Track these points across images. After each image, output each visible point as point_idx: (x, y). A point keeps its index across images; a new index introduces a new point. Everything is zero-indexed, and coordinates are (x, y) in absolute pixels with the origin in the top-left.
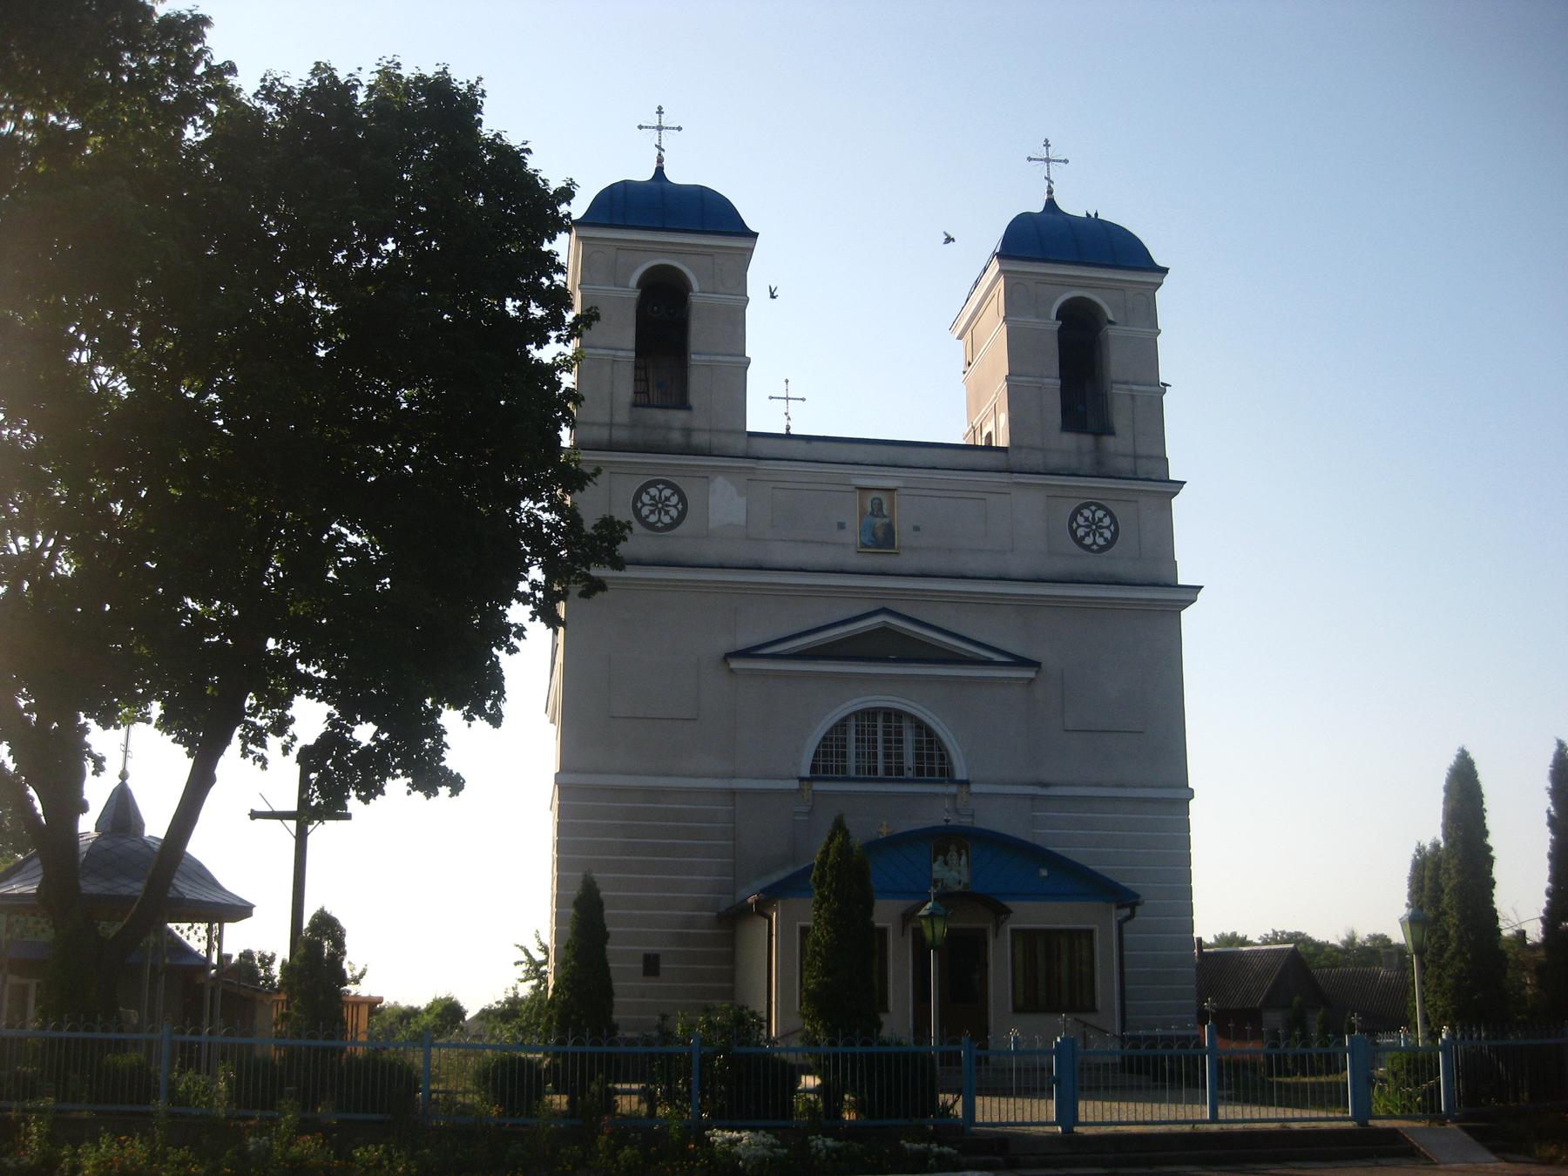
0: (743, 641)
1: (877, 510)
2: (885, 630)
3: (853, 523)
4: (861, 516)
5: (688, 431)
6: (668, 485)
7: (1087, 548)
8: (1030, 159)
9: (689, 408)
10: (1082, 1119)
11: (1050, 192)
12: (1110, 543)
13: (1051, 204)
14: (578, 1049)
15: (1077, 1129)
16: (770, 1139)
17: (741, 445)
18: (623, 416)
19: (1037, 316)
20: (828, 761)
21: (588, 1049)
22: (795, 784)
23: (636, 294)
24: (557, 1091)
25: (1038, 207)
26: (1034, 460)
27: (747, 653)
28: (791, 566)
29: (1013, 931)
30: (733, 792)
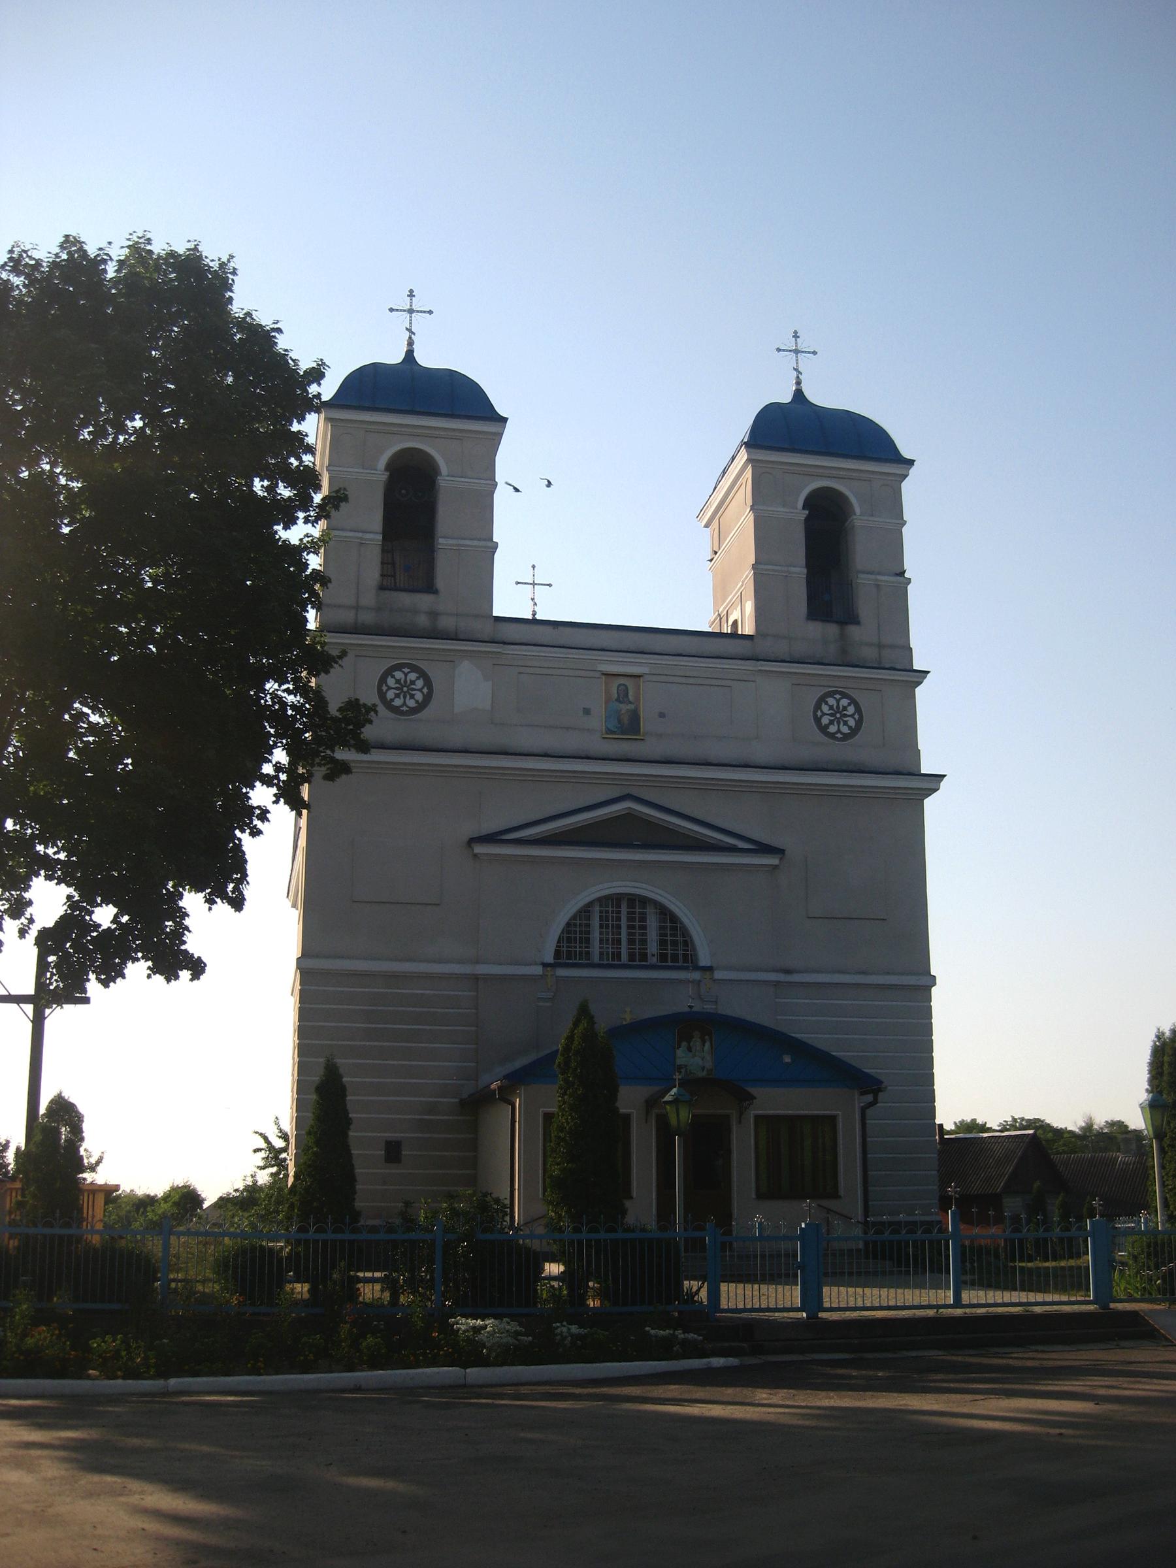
0: (490, 826)
1: (623, 696)
2: (629, 816)
4: (607, 702)
5: (434, 615)
6: (414, 669)
7: (832, 736)
8: (779, 350)
9: (436, 592)
10: (826, 1305)
11: (798, 383)
12: (854, 731)
13: (799, 395)
16: (514, 1327)
17: (487, 630)
18: (369, 598)
22: (539, 970)
23: (384, 477)
27: (491, 838)
29: (757, 1117)
30: (476, 978)
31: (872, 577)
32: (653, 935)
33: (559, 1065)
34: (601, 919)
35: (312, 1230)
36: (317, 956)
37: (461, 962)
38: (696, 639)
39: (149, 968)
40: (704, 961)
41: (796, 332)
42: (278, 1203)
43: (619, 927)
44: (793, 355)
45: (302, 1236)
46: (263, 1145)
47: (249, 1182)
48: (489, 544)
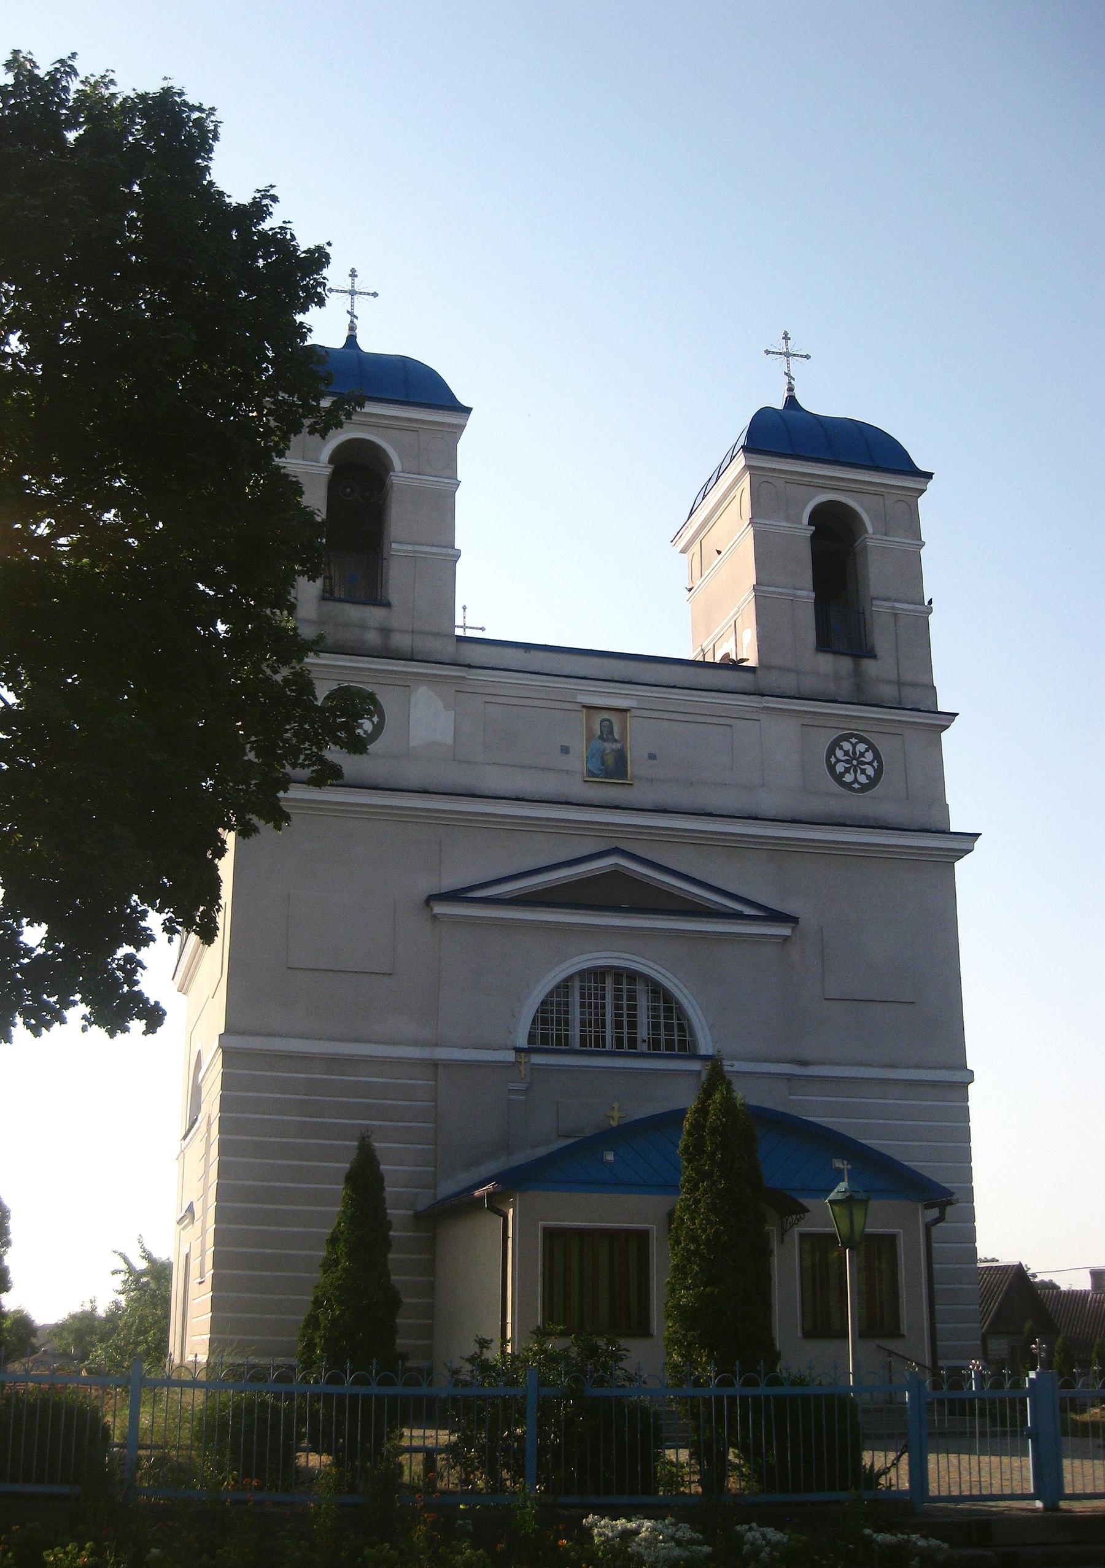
0: (451, 881)
1: (607, 734)
2: (616, 875)
3: (579, 747)
5: (385, 632)
7: (848, 786)
8: (768, 352)
9: (387, 605)
10: (1068, 1490)
11: (791, 389)
12: (873, 781)
13: (791, 402)
14: (361, 1390)
15: (1063, 1504)
16: (685, 1532)
17: (449, 650)
19: (788, 519)
20: (550, 1028)
21: (374, 1389)
22: (511, 1056)
23: (328, 471)
24: (315, 1449)
25: (779, 404)
26: (788, 683)
27: (455, 896)
28: (507, 795)
29: (803, 1236)
30: (435, 1064)
31: (890, 604)
32: (643, 1018)
33: (686, 1147)
34: (582, 996)
35: (349, 1379)
36: (244, 1033)
37: (416, 1043)
38: (691, 670)
39: (84, 1017)
40: (705, 1047)
41: (786, 333)
42: (139, 1332)
43: (603, 1007)
44: (783, 358)
45: (331, 1389)
46: (124, 1267)
47: (88, 1307)
48: (451, 551)
